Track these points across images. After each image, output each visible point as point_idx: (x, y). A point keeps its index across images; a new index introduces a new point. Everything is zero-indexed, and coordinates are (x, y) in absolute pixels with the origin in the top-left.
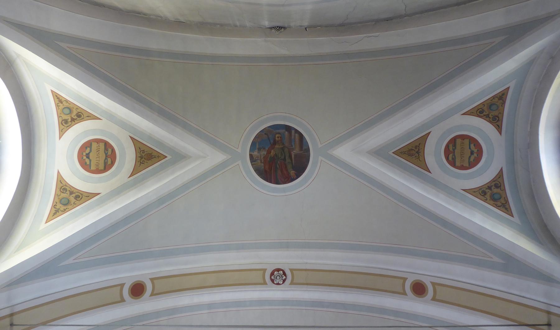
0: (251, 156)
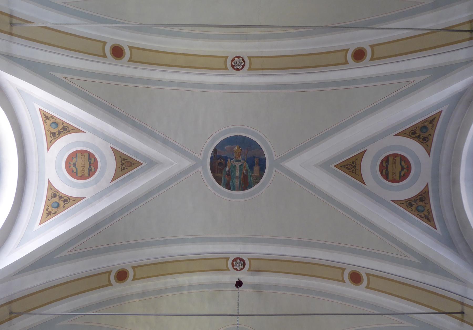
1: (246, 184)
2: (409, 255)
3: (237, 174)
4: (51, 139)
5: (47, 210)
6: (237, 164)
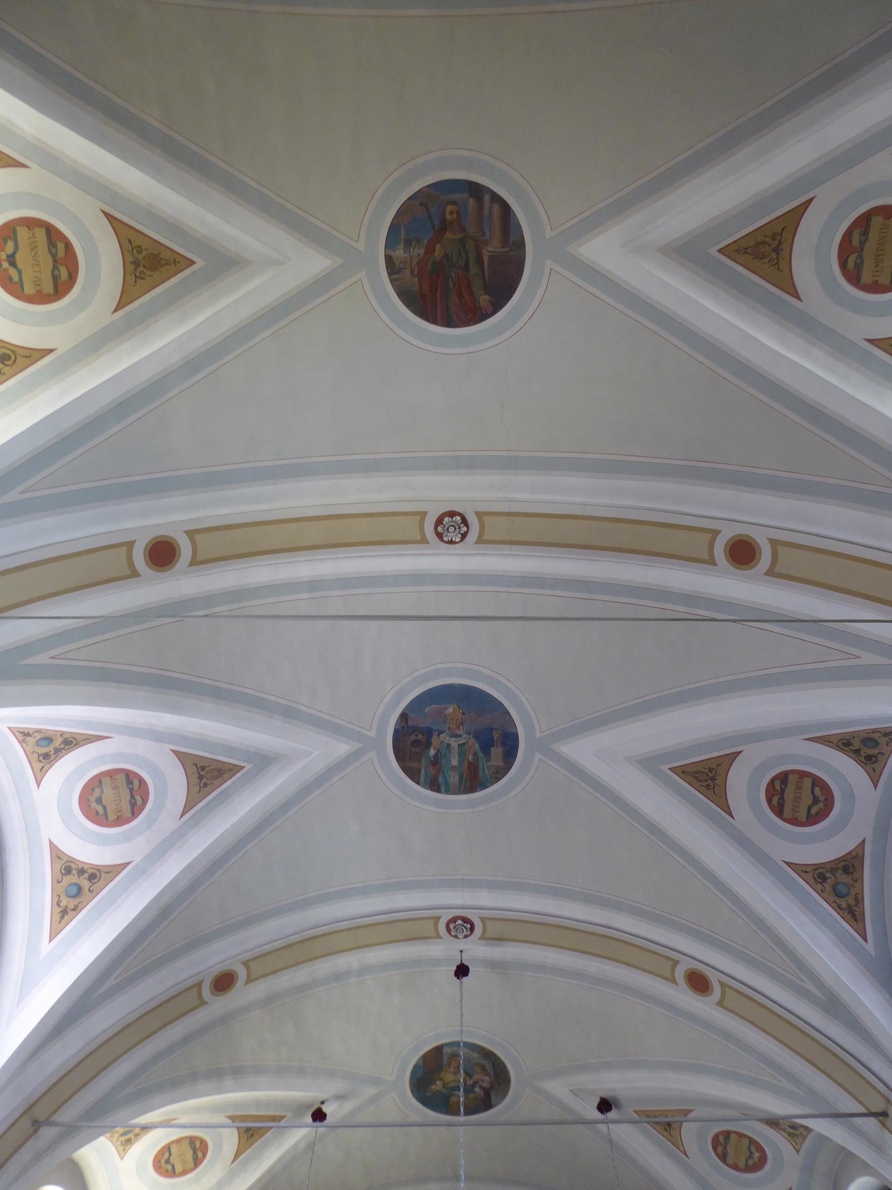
0: (389, 260)
1: (472, 781)
2: (803, 977)
3: (455, 762)
4: (41, 765)
5: (59, 905)
6: (454, 743)
